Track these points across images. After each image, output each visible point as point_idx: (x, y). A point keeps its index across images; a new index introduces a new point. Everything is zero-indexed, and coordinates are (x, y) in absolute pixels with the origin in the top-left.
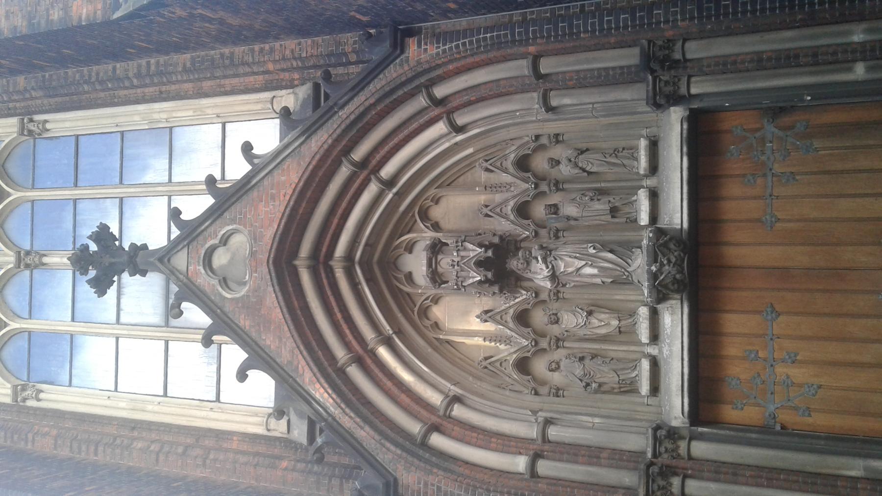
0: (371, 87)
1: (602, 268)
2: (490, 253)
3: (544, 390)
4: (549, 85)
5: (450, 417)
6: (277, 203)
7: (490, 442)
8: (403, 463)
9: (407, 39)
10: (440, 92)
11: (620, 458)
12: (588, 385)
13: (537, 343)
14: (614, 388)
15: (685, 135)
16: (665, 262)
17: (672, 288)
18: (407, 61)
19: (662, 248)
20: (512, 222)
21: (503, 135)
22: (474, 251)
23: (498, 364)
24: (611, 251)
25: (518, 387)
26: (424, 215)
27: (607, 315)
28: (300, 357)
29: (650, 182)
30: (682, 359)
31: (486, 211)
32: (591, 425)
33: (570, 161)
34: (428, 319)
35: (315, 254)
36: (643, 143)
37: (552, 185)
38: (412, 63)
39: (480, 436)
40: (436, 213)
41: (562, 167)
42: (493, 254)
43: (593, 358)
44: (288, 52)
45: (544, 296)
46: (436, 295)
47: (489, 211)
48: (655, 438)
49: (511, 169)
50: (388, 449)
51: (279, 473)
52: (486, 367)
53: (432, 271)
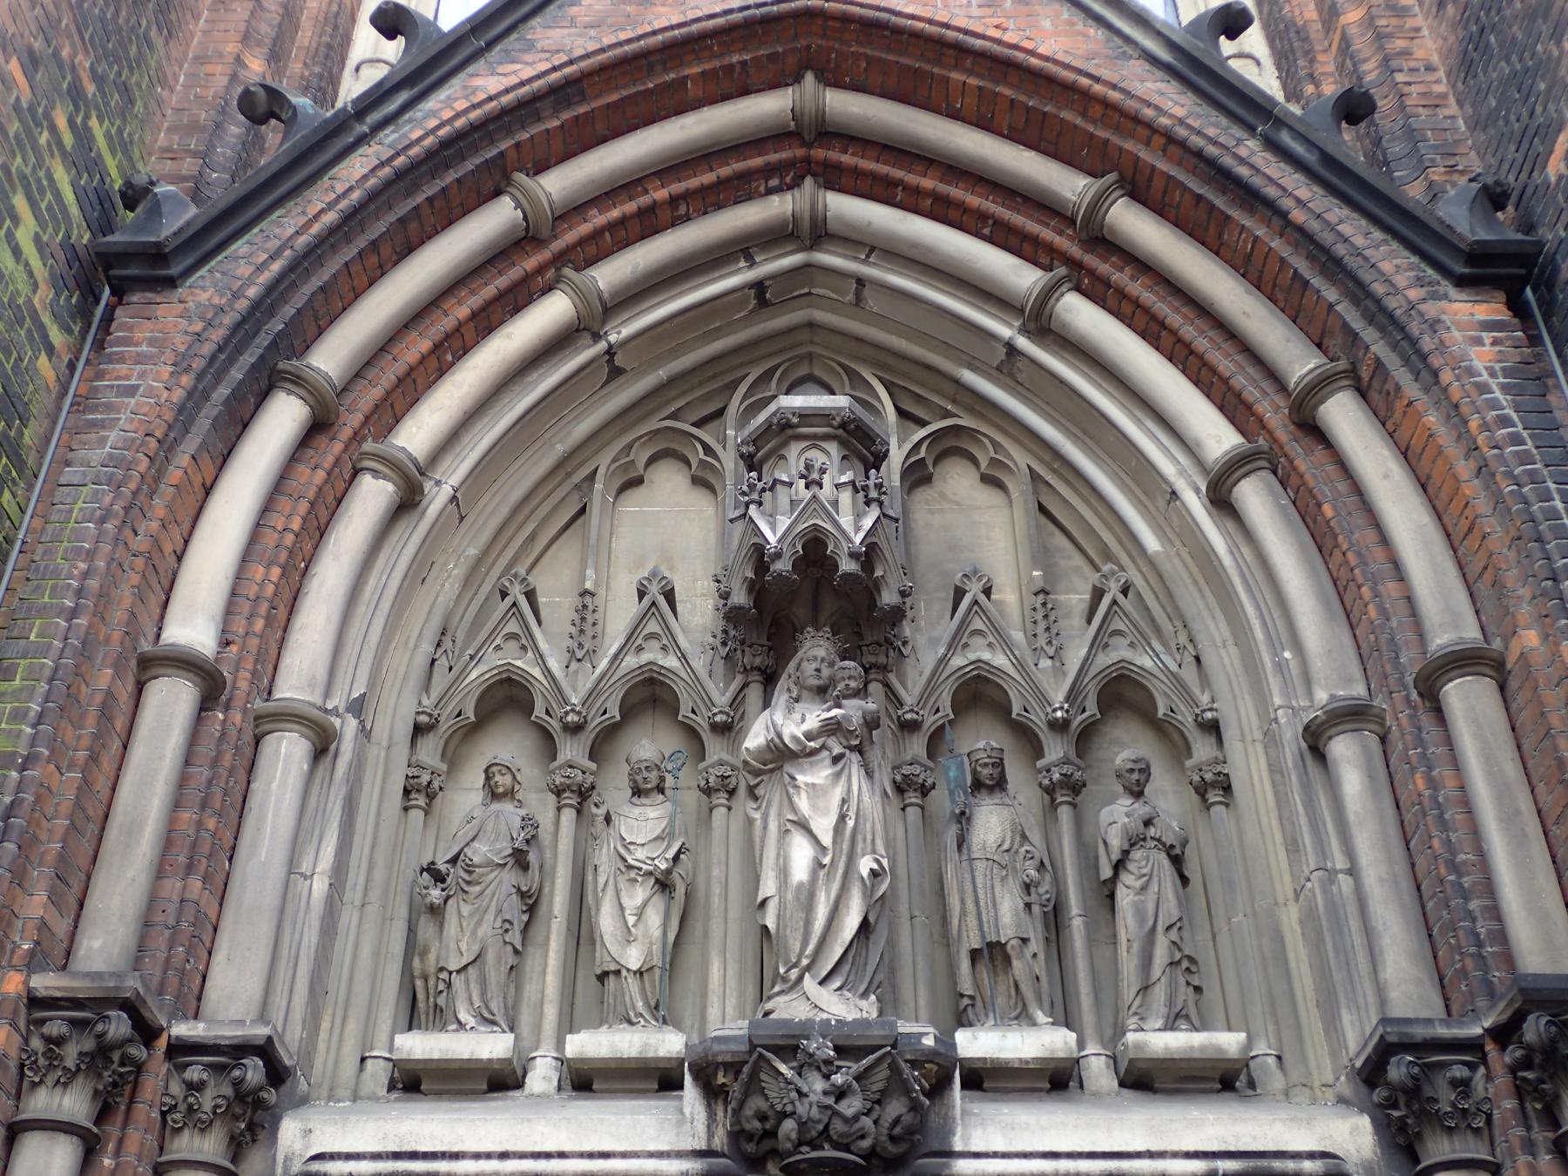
0: (1337, 212)
1: (812, 895)
2: (847, 566)
3: (429, 752)
4: (1399, 722)
5: (356, 472)
6: (975, 12)
7: (268, 567)
8: (216, 301)
9: (1502, 296)
10: (1343, 415)
11: (184, 930)
12: (439, 878)
13: (575, 729)
14: (423, 954)
15: (1278, 1165)
16: (838, 1079)
17: (748, 1111)
18: (1435, 296)
19: (882, 1073)
20: (943, 661)
21: (1213, 632)
22: (852, 525)
23: (513, 627)
24: (865, 927)
25: (441, 680)
26: (950, 445)
27: (656, 933)
28: (546, 66)
29: (1098, 1070)
30: (504, 1156)
31: (974, 590)
32: (305, 867)
33: (1148, 823)
34: (651, 462)
35: (827, 132)
36: (1229, 1042)
37: (1066, 769)
38: (1431, 309)
39: (289, 539)
40: (958, 481)
41: (1124, 804)
42: (847, 575)
43: (523, 895)
44: (1400, 44)
45: (716, 750)
46: (720, 474)
47: (968, 598)
48: (241, 1050)
49: (1104, 660)
50: (260, 268)
51: (231, 48)
52: (504, 595)
53: (789, 425)
